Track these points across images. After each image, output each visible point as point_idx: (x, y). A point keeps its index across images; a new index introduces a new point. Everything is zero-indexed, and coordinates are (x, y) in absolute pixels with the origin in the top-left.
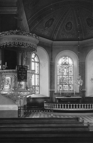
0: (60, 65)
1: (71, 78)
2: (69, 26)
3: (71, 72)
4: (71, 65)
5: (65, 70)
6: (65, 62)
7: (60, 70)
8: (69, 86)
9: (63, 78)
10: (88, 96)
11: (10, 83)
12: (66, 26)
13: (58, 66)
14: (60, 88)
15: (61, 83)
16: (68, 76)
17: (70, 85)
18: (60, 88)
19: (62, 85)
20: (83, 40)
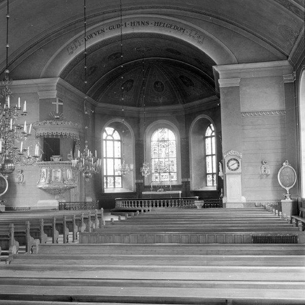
0: (155, 142)
1: (172, 161)
2: (159, 86)
3: (173, 152)
4: (172, 142)
5: (164, 149)
6: (163, 137)
7: (155, 150)
8: (170, 175)
9: (161, 162)
10: (193, 190)
11: (45, 176)
12: (155, 87)
13: (152, 144)
14: (156, 178)
15: (157, 169)
16: (168, 159)
17: (171, 174)
18: (156, 178)
19: (159, 173)
20: (39, 78)
